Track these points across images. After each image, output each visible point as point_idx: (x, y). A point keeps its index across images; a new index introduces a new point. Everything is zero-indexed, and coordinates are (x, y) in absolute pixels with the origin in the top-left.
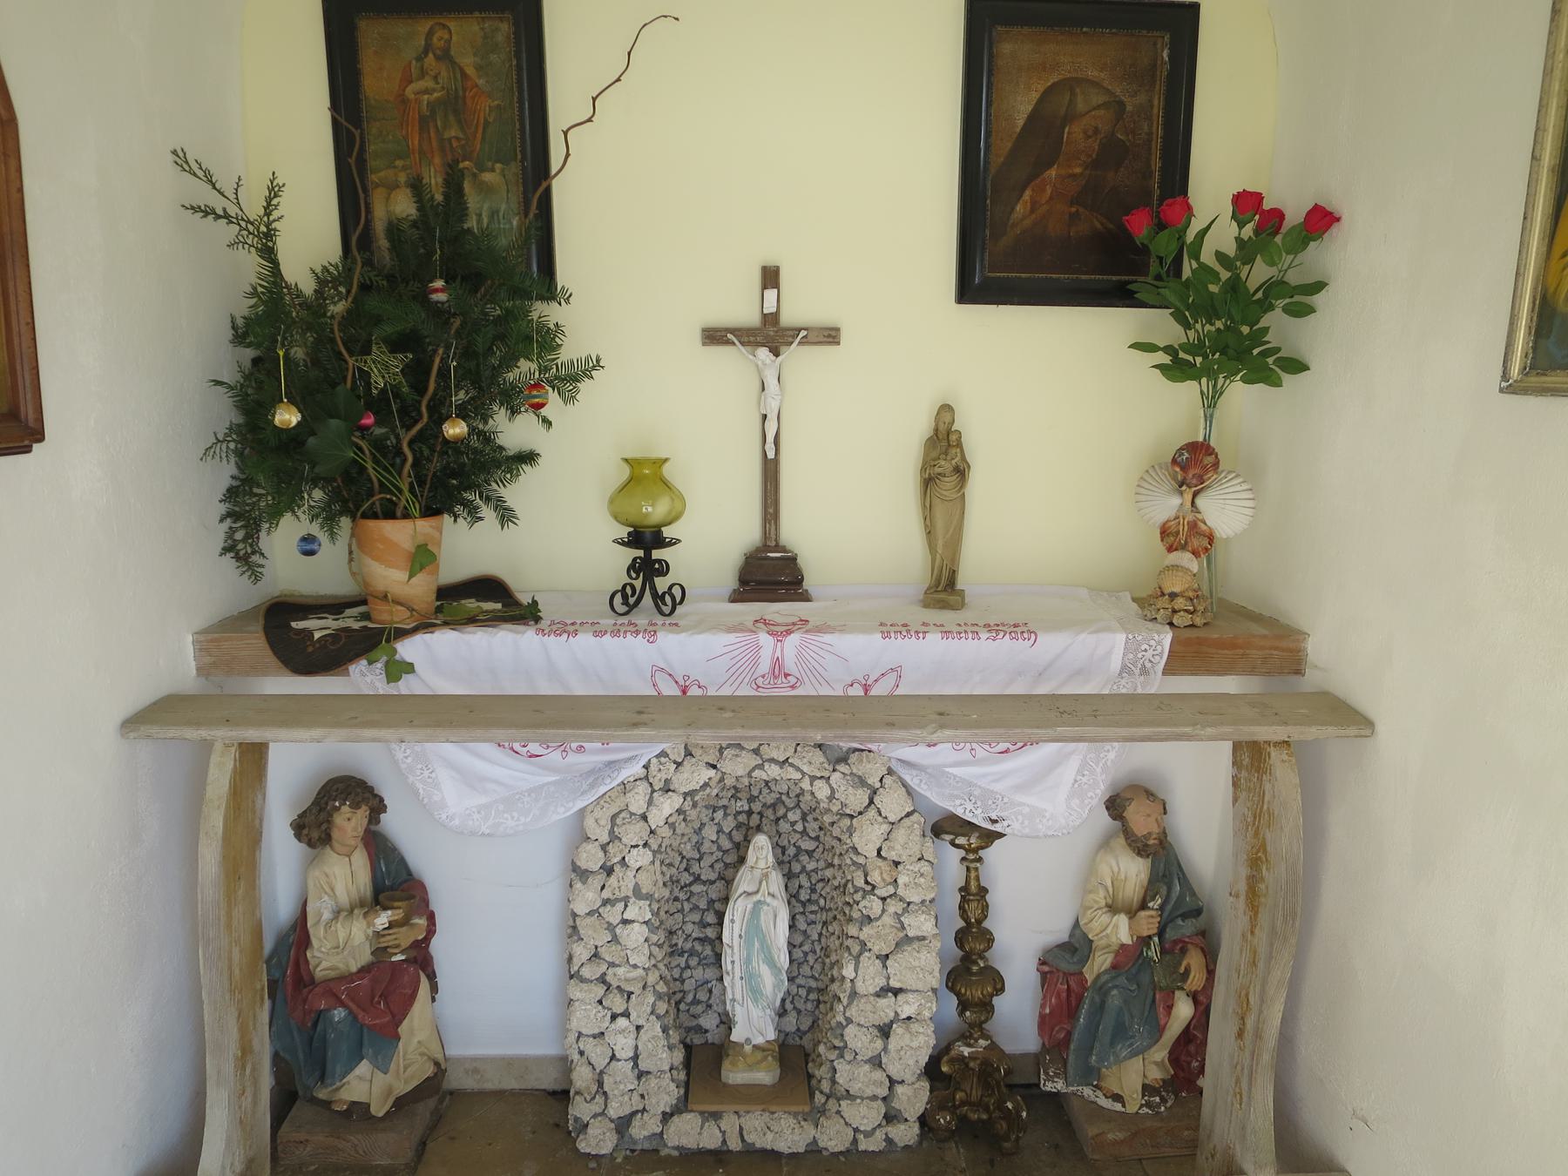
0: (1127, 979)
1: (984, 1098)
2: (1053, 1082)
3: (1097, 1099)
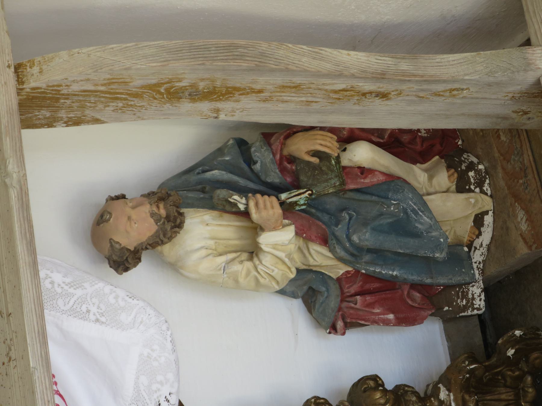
0: (337, 225)
1: (508, 383)
2: (473, 299)
3: (484, 245)
